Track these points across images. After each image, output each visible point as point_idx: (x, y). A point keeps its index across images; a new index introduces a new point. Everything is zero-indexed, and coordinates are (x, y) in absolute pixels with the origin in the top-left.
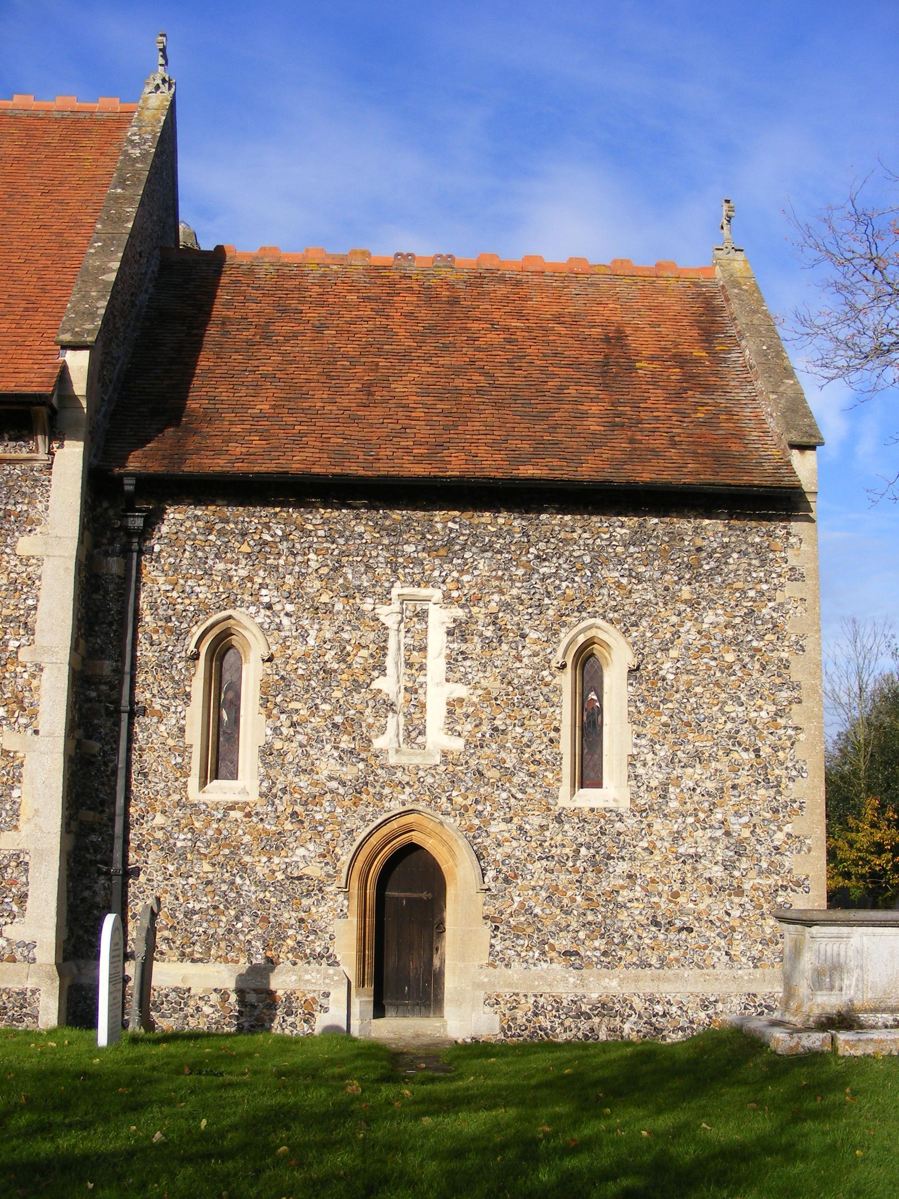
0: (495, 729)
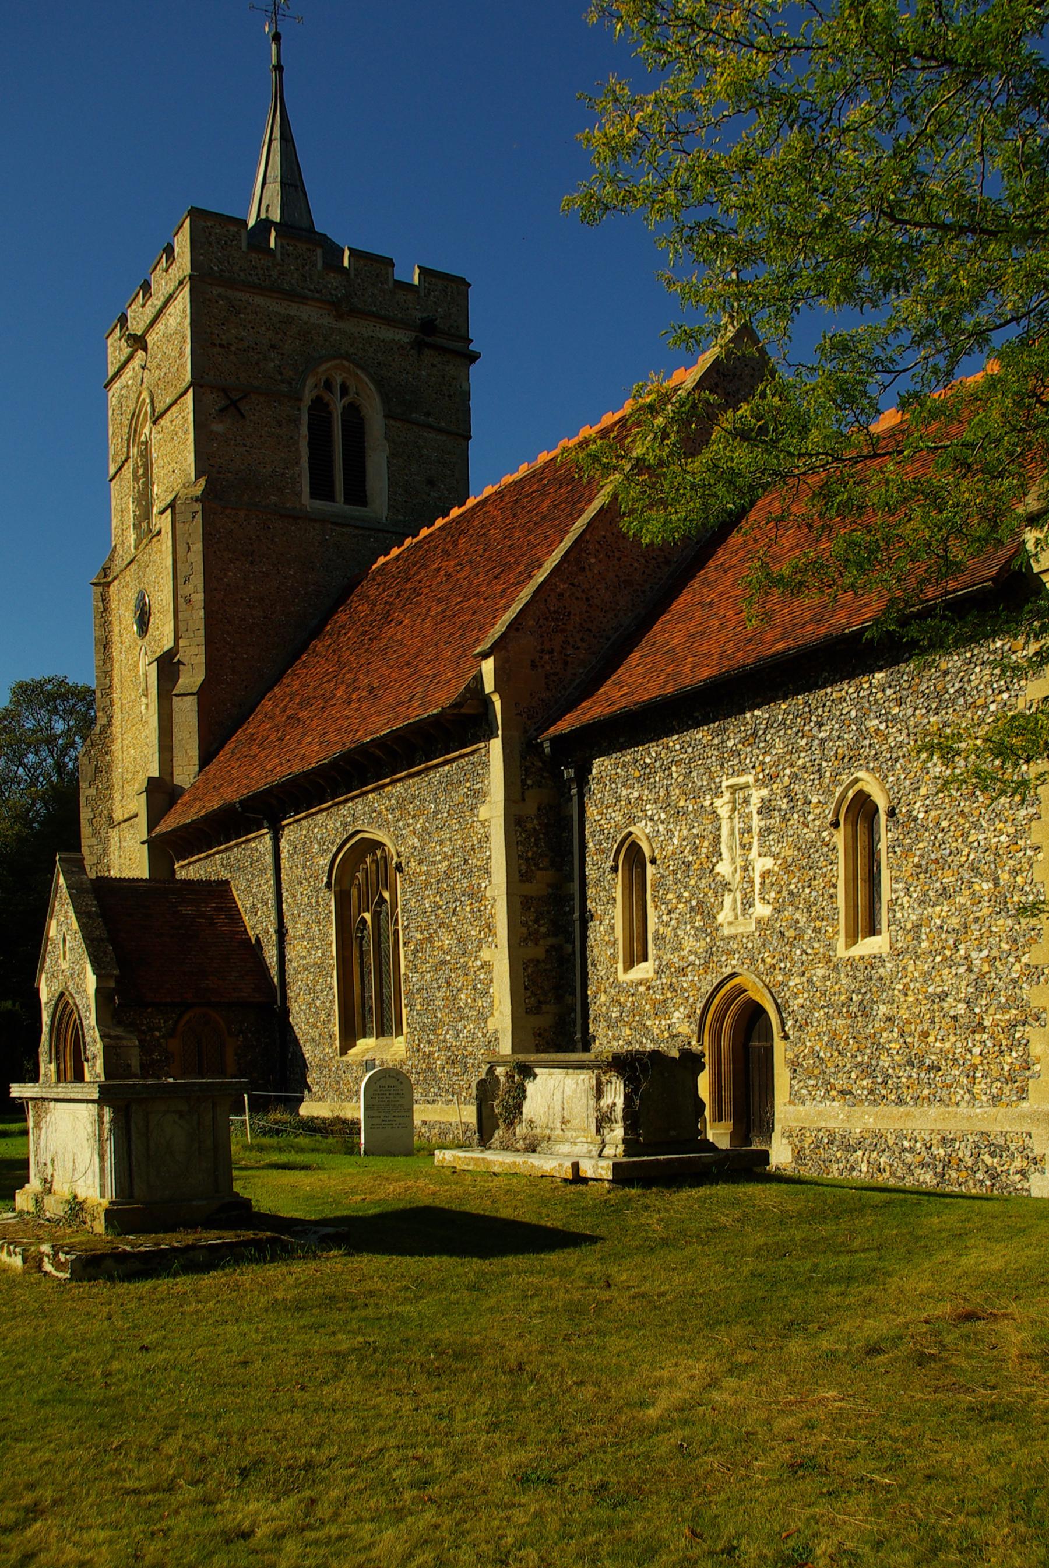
0: (791, 893)
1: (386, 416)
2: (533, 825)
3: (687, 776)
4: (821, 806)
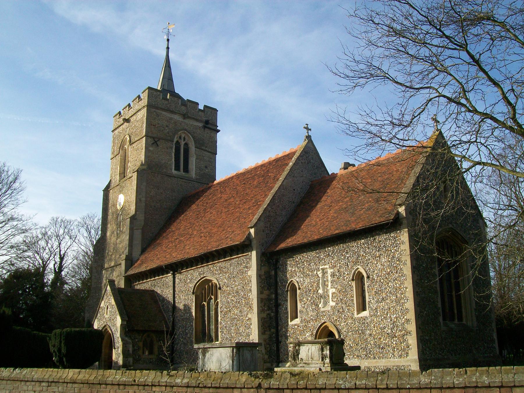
1: (195, 147)
2: (263, 277)
3: (309, 265)
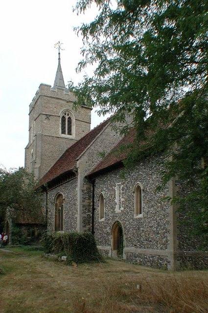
4: (132, 189)
